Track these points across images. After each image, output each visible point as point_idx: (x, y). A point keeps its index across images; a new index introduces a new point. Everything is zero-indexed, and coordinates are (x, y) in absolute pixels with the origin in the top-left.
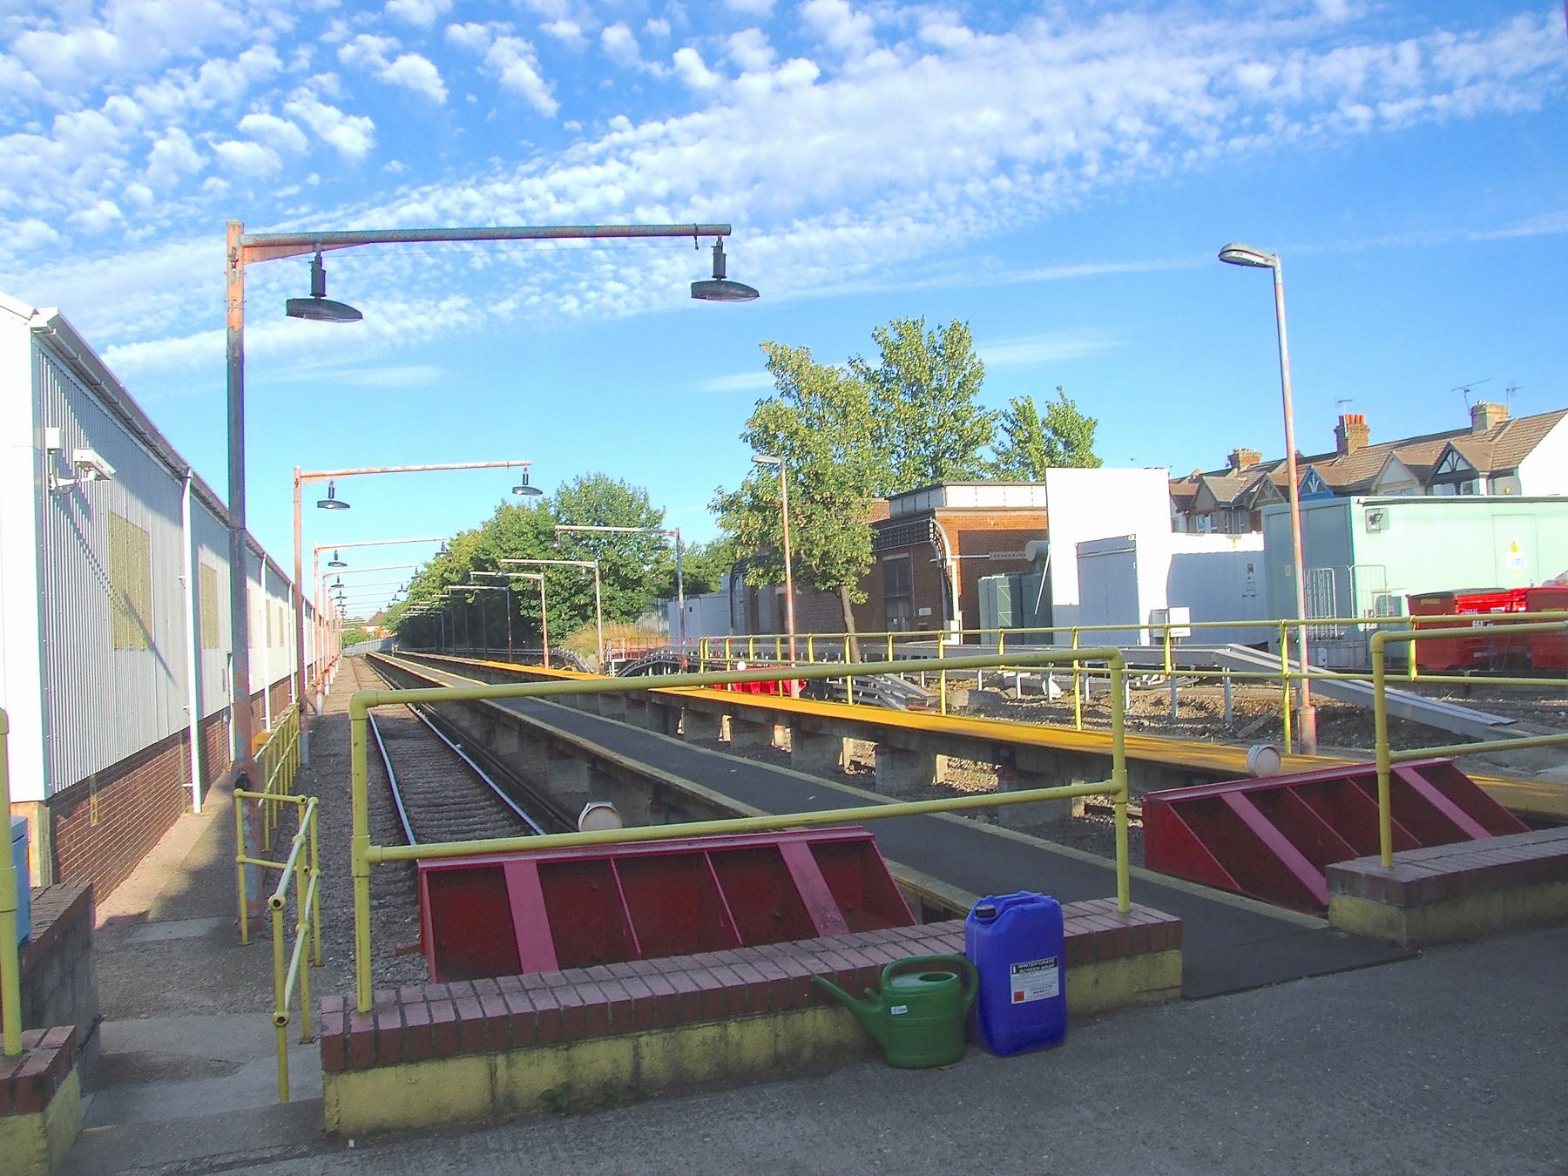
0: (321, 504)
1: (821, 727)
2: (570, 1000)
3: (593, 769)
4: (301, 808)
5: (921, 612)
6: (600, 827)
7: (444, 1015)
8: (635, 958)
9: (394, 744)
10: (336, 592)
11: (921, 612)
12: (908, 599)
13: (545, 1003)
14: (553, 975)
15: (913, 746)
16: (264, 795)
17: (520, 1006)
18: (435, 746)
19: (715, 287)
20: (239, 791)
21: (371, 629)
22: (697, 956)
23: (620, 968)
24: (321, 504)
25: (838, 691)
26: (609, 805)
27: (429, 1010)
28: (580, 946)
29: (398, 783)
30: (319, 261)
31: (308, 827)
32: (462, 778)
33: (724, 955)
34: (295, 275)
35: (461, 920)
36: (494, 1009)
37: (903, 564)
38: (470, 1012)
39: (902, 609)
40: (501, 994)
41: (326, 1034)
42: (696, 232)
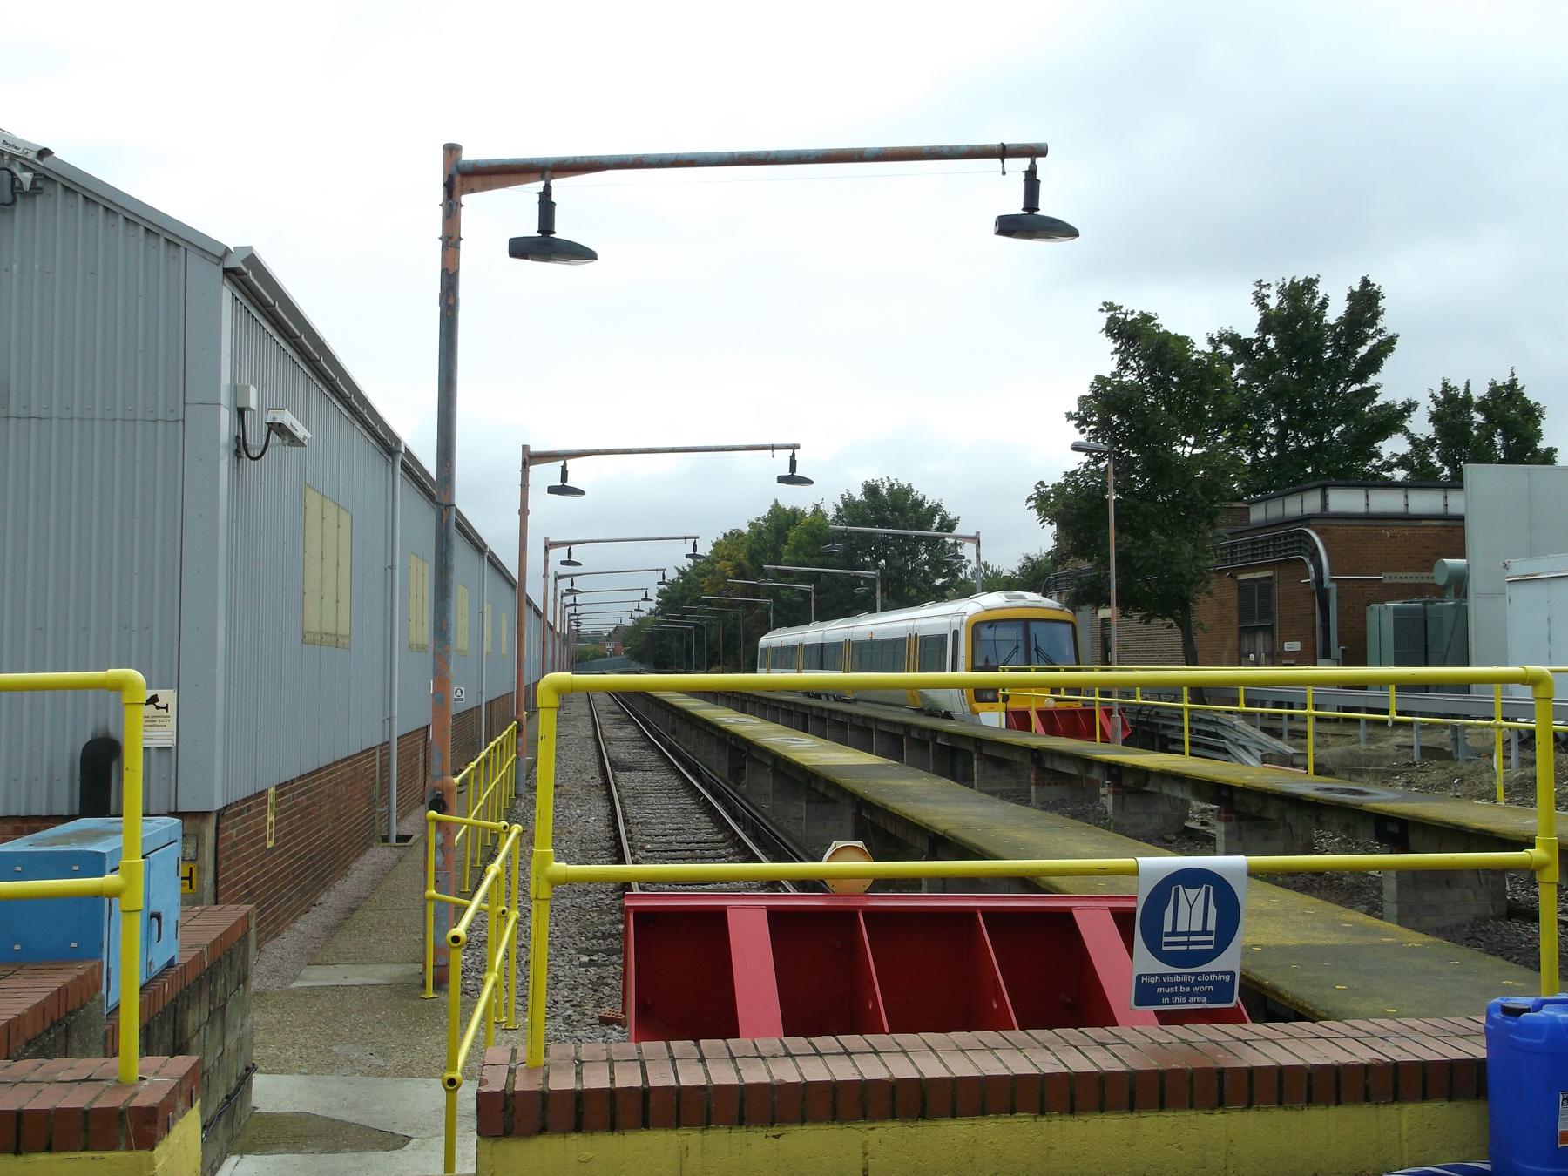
0: (552, 490)
1: (1146, 782)
2: (786, 1073)
3: (858, 818)
4: (502, 836)
5: (1288, 646)
6: (846, 864)
7: (628, 1078)
8: (878, 1030)
9: (623, 777)
10: (569, 600)
11: (1288, 646)
12: (1269, 630)
13: (755, 1074)
14: (771, 1043)
15: (1272, 814)
16: (471, 820)
17: (723, 1075)
18: (674, 782)
19: (1026, 224)
20: (433, 813)
21: (610, 646)
22: (953, 1035)
23: (853, 1041)
24: (552, 490)
25: (1175, 741)
26: (859, 844)
27: (612, 1072)
28: (812, 1009)
29: (626, 822)
30: (547, 188)
31: (509, 857)
32: (705, 822)
33: (988, 1036)
34: (514, 209)
35: (672, 969)
36: (691, 1076)
37: (1266, 584)
38: (660, 1078)
39: (1260, 640)
40: (702, 1060)
41: (484, 1089)
42: (1003, 152)
